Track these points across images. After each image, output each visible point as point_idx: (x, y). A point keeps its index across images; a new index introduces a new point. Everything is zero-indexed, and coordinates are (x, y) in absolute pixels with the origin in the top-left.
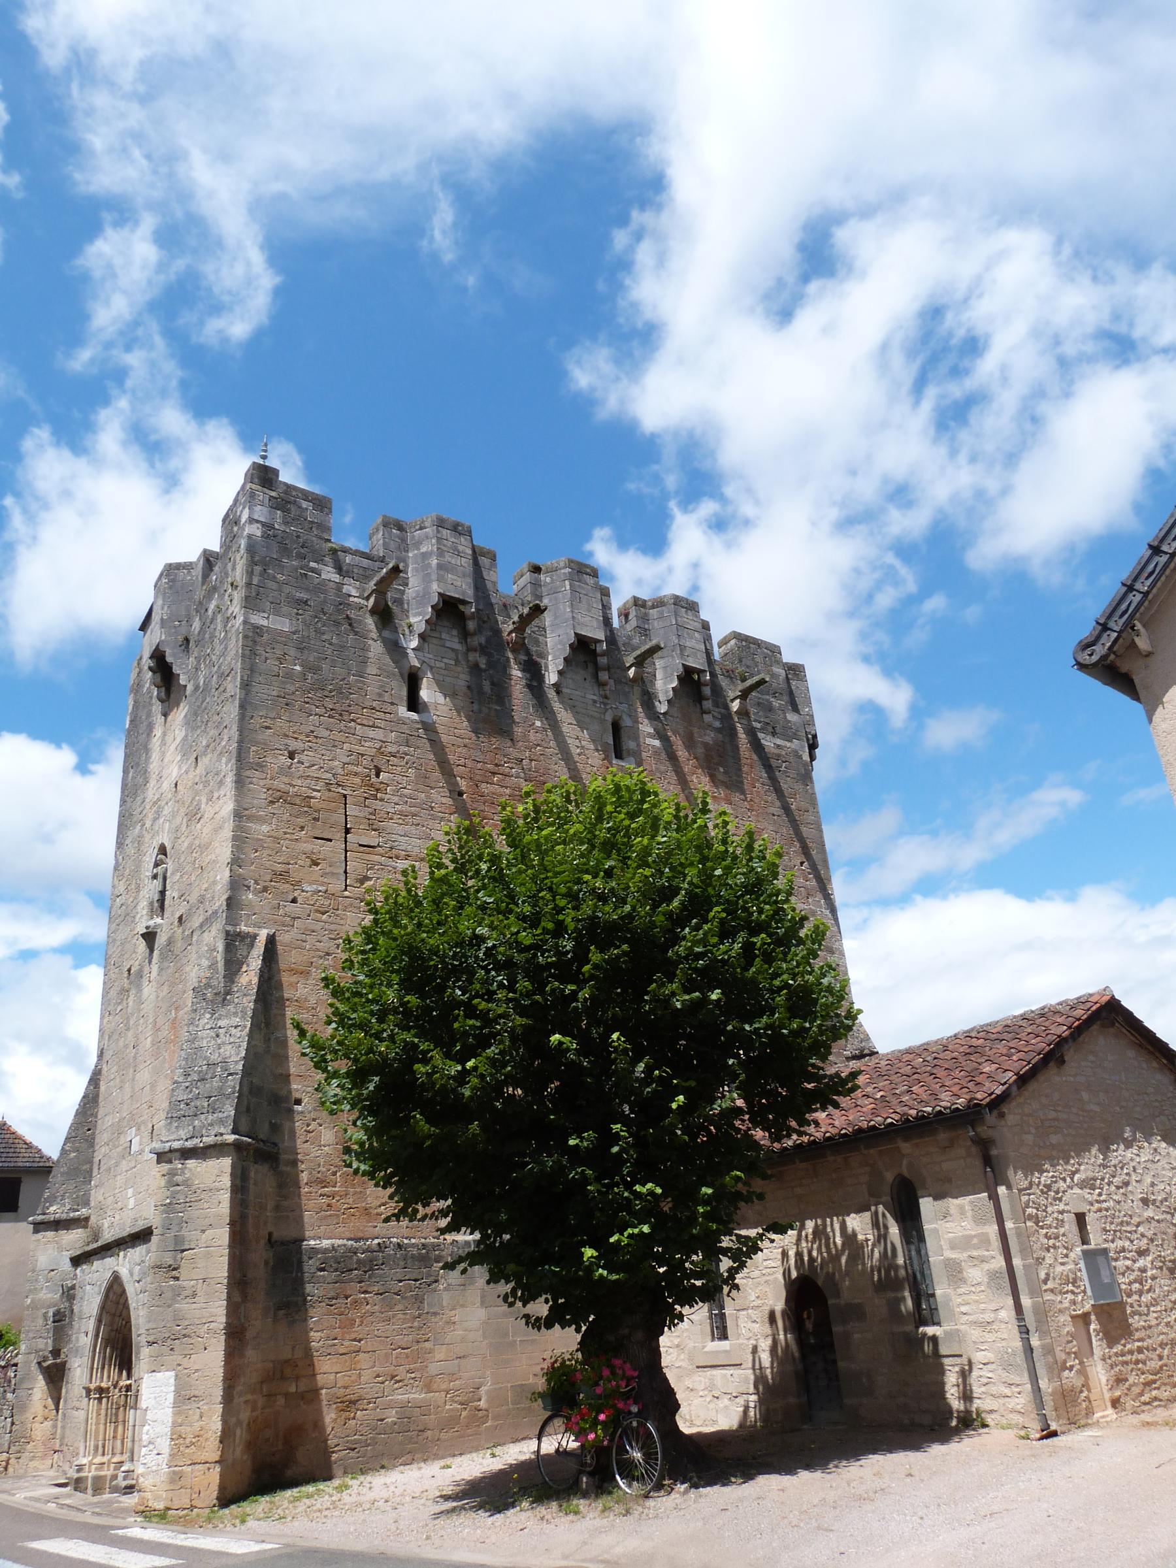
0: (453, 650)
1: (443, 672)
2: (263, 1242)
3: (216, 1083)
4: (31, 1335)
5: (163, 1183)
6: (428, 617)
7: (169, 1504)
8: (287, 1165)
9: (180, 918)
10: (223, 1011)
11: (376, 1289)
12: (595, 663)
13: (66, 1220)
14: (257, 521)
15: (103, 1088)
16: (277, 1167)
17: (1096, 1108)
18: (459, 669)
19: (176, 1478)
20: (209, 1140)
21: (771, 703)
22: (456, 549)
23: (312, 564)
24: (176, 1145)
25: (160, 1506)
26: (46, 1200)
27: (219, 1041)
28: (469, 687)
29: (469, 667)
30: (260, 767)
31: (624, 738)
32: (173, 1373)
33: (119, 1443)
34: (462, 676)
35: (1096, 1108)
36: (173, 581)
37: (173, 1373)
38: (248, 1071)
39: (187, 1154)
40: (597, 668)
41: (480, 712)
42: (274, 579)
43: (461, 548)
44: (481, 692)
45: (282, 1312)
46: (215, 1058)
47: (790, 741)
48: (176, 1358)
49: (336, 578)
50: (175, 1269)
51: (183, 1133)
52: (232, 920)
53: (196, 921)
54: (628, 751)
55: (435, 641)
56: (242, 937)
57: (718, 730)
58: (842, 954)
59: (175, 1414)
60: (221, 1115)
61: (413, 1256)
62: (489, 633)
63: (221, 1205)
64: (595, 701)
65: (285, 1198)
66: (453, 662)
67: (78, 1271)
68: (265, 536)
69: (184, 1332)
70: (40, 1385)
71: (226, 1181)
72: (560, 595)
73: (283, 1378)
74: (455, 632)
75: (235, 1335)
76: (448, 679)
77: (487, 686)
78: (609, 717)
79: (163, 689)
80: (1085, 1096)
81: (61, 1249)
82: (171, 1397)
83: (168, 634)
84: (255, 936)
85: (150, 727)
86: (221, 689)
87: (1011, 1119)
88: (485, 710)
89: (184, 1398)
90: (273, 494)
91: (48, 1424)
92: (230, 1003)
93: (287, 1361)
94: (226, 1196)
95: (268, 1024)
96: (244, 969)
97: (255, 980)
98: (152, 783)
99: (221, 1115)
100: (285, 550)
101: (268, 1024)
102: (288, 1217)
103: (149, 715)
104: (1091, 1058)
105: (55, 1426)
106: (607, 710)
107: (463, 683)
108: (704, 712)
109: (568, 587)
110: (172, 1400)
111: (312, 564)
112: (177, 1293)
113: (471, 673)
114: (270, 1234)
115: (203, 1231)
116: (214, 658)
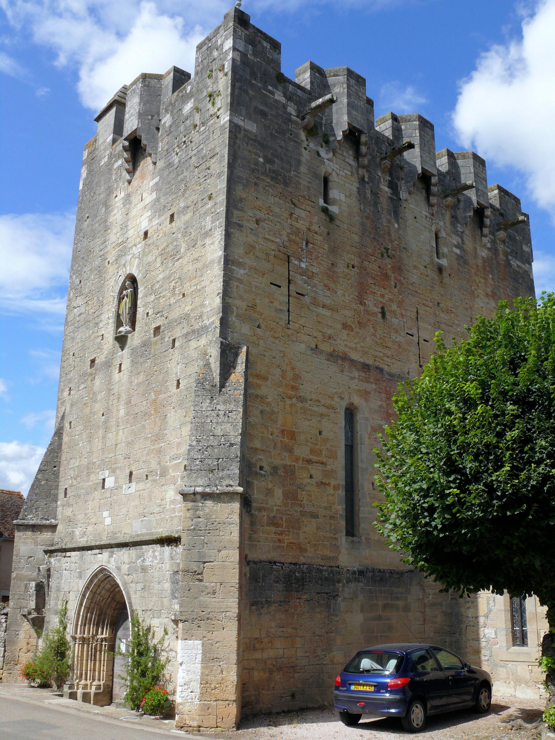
0: (350, 165)
1: (344, 179)
4: (17, 597)
7: (201, 724)
8: (255, 511)
11: (305, 597)
13: (40, 525)
14: (238, 50)
15: (65, 439)
16: (250, 511)
18: (353, 179)
19: (205, 709)
22: (358, 95)
23: (270, 88)
25: (195, 724)
26: (25, 510)
29: (358, 178)
31: (441, 245)
34: (355, 184)
37: (200, 642)
38: (243, 443)
39: (205, 496)
42: (247, 93)
45: (254, 607)
47: (524, 264)
49: (283, 100)
50: (198, 574)
57: (489, 249)
59: (203, 668)
60: (229, 472)
63: (233, 534)
64: (426, 217)
66: (350, 173)
69: (208, 616)
73: (255, 649)
74: (351, 153)
76: (347, 185)
78: (434, 229)
79: (131, 164)
82: (199, 657)
89: (209, 658)
93: (256, 639)
97: (242, 380)
99: (229, 472)
100: (253, 74)
102: (256, 545)
106: (433, 224)
108: (482, 235)
109: (418, 135)
110: (200, 660)
111: (270, 88)
115: (219, 551)
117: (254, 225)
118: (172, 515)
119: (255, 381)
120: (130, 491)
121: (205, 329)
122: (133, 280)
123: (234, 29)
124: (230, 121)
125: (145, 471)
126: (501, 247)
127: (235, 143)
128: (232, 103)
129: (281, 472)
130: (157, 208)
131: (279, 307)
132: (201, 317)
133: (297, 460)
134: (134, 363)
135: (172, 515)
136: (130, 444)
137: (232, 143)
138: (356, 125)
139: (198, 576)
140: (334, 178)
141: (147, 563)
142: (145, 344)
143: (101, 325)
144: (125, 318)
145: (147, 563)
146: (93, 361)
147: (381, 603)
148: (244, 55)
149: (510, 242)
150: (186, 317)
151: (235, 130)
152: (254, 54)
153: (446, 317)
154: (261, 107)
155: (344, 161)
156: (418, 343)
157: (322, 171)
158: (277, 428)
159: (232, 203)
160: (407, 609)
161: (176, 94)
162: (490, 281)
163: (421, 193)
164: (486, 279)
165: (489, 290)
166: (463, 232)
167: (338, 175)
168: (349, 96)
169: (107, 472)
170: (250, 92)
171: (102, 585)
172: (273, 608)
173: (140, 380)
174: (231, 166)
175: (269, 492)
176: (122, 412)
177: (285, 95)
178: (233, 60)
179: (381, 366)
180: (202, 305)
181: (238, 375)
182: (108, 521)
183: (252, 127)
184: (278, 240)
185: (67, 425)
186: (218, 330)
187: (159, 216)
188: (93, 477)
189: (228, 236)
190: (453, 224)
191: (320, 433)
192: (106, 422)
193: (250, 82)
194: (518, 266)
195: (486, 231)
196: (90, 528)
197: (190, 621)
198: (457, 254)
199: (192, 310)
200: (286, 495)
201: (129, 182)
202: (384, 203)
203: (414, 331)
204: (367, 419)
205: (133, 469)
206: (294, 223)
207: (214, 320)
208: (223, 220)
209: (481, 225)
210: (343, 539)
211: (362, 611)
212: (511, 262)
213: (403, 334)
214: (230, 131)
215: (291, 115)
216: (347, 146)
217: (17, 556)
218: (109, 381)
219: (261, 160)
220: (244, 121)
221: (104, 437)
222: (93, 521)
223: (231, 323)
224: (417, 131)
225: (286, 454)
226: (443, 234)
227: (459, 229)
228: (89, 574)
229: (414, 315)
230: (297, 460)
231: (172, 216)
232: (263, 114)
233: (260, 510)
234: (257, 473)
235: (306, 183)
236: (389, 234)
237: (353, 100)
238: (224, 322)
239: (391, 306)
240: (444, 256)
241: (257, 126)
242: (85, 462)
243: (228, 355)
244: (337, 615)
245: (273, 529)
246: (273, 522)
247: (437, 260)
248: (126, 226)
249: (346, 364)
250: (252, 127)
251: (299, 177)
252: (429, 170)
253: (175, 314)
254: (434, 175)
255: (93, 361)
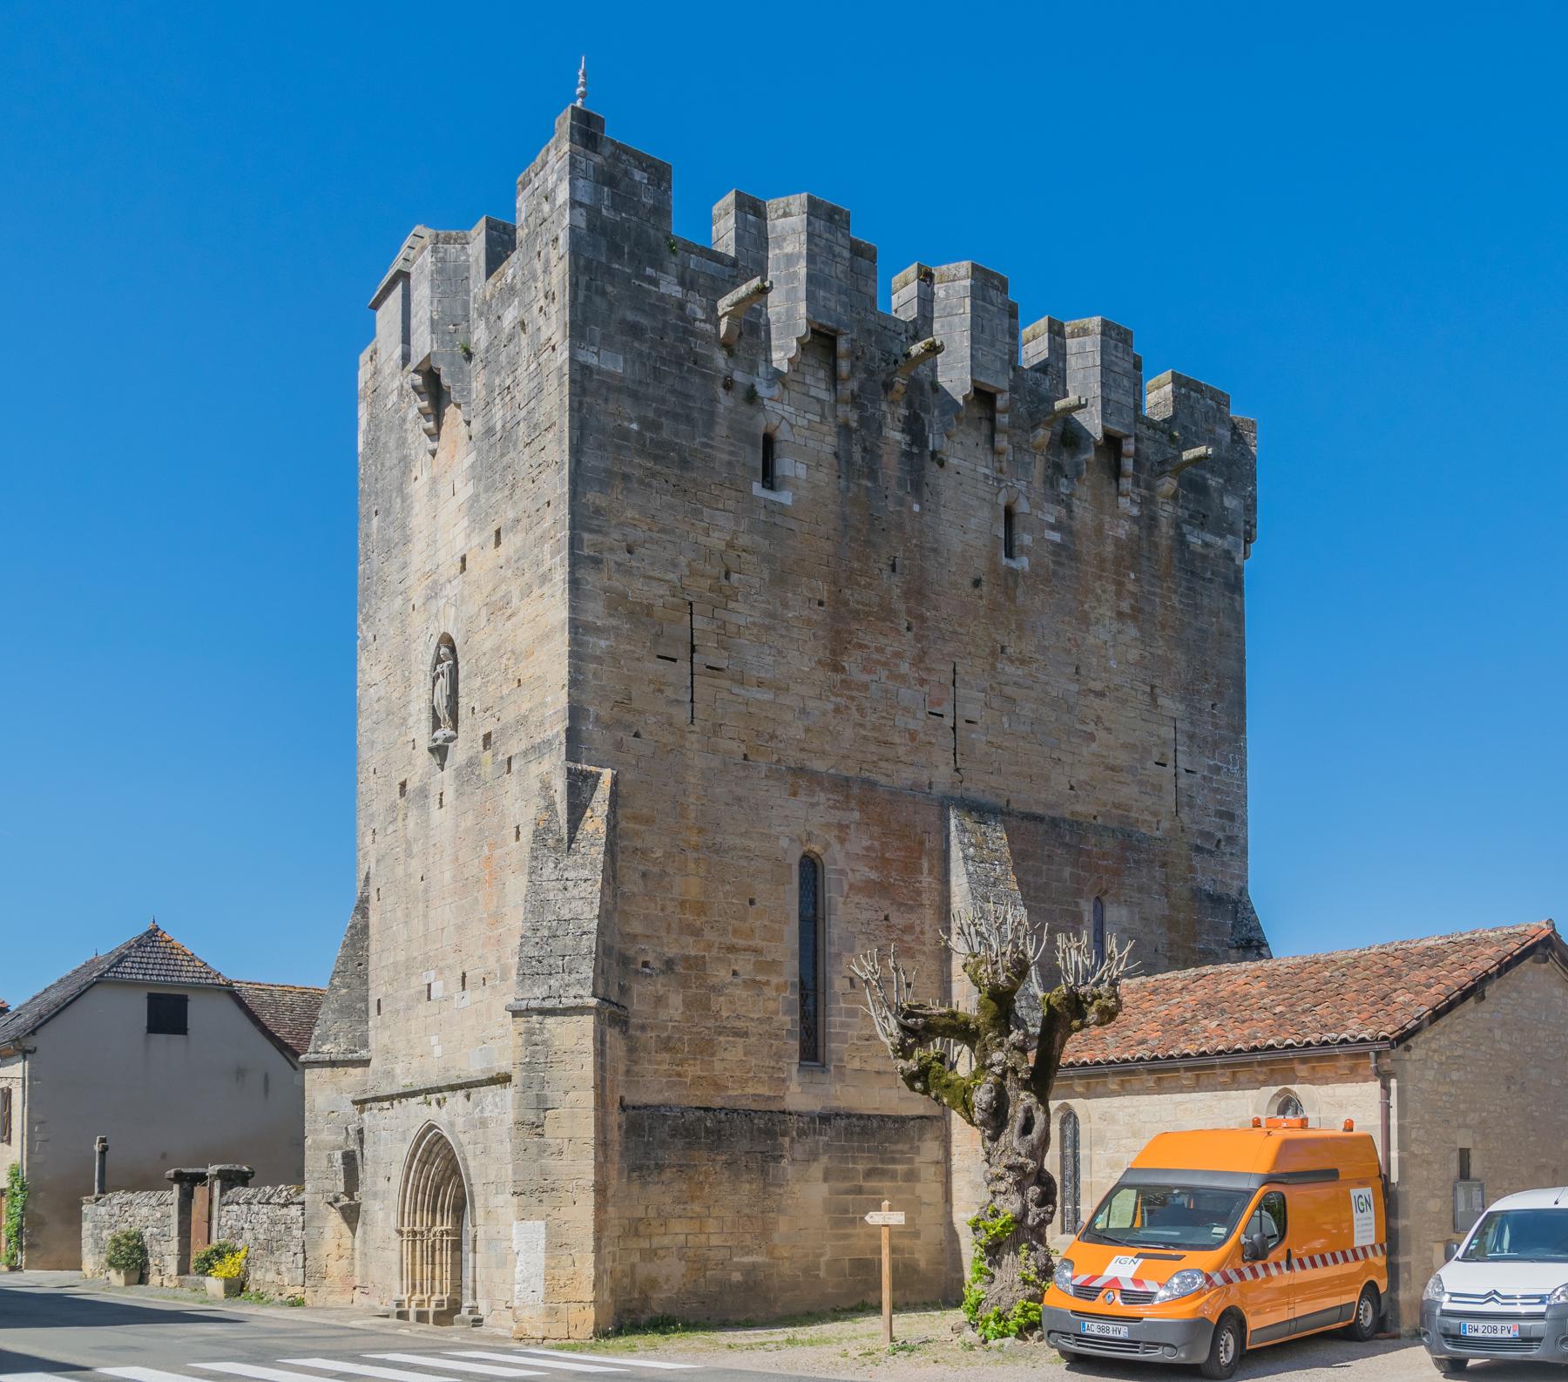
0: (818, 400)
1: (806, 433)
2: (617, 1105)
3: (569, 941)
4: (316, 1175)
5: (520, 1041)
6: (792, 354)
9: (487, 737)
10: (569, 861)
12: (992, 420)
15: (374, 918)
17: (1506, 1047)
18: (825, 428)
20: (570, 1002)
21: (1205, 479)
23: (649, 271)
24: (534, 1004)
27: (568, 895)
28: (836, 454)
30: (596, 562)
31: (1018, 529)
32: (542, 1223)
33: (437, 1283)
34: (829, 439)
35: (1506, 1047)
36: (443, 260)
37: (542, 1223)
38: (601, 931)
40: (993, 430)
41: (848, 489)
42: (604, 294)
43: (837, 249)
44: (850, 463)
46: (565, 913)
47: (1222, 536)
48: (545, 1208)
49: (676, 291)
51: (540, 991)
52: (572, 755)
53: (515, 746)
54: (1022, 548)
55: (797, 387)
56: (586, 776)
57: (1135, 520)
58: (1244, 823)
61: (759, 1129)
62: (864, 376)
64: (987, 477)
65: (636, 1062)
66: (817, 419)
67: (365, 1115)
68: (591, 228)
70: (334, 1219)
71: (589, 1044)
72: (956, 319)
74: (822, 374)
75: (600, 1190)
76: (811, 444)
77: (857, 454)
78: (1002, 501)
80: (1498, 1034)
81: (340, 1091)
82: (542, 1243)
83: (442, 343)
84: (599, 774)
85: (405, 463)
86: (536, 446)
87: (1416, 1053)
88: (853, 487)
90: (598, 159)
91: (344, 1262)
92: (577, 852)
93: (641, 1219)
94: (589, 1061)
95: (614, 878)
96: (589, 813)
97: (603, 828)
98: (418, 545)
100: (615, 250)
101: (614, 878)
103: (402, 442)
104: (1514, 995)
105: (352, 1264)
107: (828, 449)
108: (1119, 493)
109: (968, 309)
112: (542, 1150)
113: (839, 433)
114: (622, 1099)
115: (566, 1093)
116: (519, 397)
117: (623, 556)
118: (502, 1046)
119: (631, 825)
120: (466, 1002)
121: (548, 743)
122: (447, 641)
123: (571, 157)
124: (572, 359)
125: (480, 972)
126: (1166, 511)
127: (581, 403)
128: (572, 323)
129: (679, 969)
130: (476, 512)
131: (673, 697)
132: (542, 723)
133: (709, 946)
134: (459, 794)
135: (502, 1046)
136: (460, 928)
137: (576, 405)
138: (824, 322)
139: (537, 1127)
140: (783, 434)
141: (487, 1114)
142: (472, 763)
143: (411, 722)
144: (443, 713)
145: (487, 1114)
146: (403, 785)
147: (861, 1167)
148: (593, 212)
149: (1191, 496)
150: (522, 721)
151: (582, 380)
152: (614, 207)
153: (1019, 672)
154: (630, 316)
155: (807, 394)
156: (954, 729)
157: (761, 424)
158: (672, 900)
159: (581, 520)
160: (911, 1176)
161: (491, 280)
162: (1131, 587)
163: (978, 429)
164: (1120, 584)
165: (1125, 606)
166: (1071, 496)
167: (792, 426)
168: (811, 259)
169: (433, 974)
170: (609, 289)
171: (435, 1150)
172: (668, 1175)
173: (469, 824)
174: (576, 451)
175: (659, 1001)
176: (448, 875)
177: (682, 283)
178: (573, 229)
179: (874, 777)
180: (543, 704)
181: (595, 822)
182: (438, 1051)
183: (613, 364)
184: (670, 576)
185: (374, 895)
186: (563, 749)
187: (482, 529)
188: (414, 981)
189: (575, 584)
190: (1050, 482)
191: (752, 902)
192: (426, 891)
193: (610, 268)
194: (1206, 544)
195: (1126, 484)
196: (415, 1063)
197: (535, 1192)
198: (1053, 543)
199: (531, 710)
200: (688, 1004)
201: (433, 453)
202: (891, 464)
203: (946, 708)
204: (842, 872)
205: (466, 968)
206: (702, 539)
207: (557, 728)
208: (565, 553)
209: (1117, 473)
210: (792, 1065)
211: (825, 1179)
212: (1189, 538)
213: (921, 715)
214: (572, 381)
215: (695, 320)
216: (812, 362)
217: (311, 1111)
218: (425, 823)
219: (634, 426)
220: (597, 354)
221: (425, 916)
222: (418, 1051)
223: (584, 735)
224: (968, 301)
225: (691, 940)
226: (1023, 507)
227: (1063, 490)
228: (413, 1133)
229: (946, 678)
230: (709, 946)
231: (498, 533)
232: (635, 330)
233: (643, 1028)
234: (637, 972)
235: (725, 457)
236: (900, 527)
237: (819, 265)
238: (573, 735)
239: (897, 665)
240: (1025, 551)
241: (625, 361)
242: (401, 957)
243: (579, 787)
244: (781, 1186)
245: (667, 1056)
246: (666, 1045)
247: (1005, 561)
248: (435, 541)
249: (803, 783)
250: (613, 364)
251: (711, 447)
252: (990, 382)
253: (509, 715)
254: (1002, 392)
255: (403, 785)
